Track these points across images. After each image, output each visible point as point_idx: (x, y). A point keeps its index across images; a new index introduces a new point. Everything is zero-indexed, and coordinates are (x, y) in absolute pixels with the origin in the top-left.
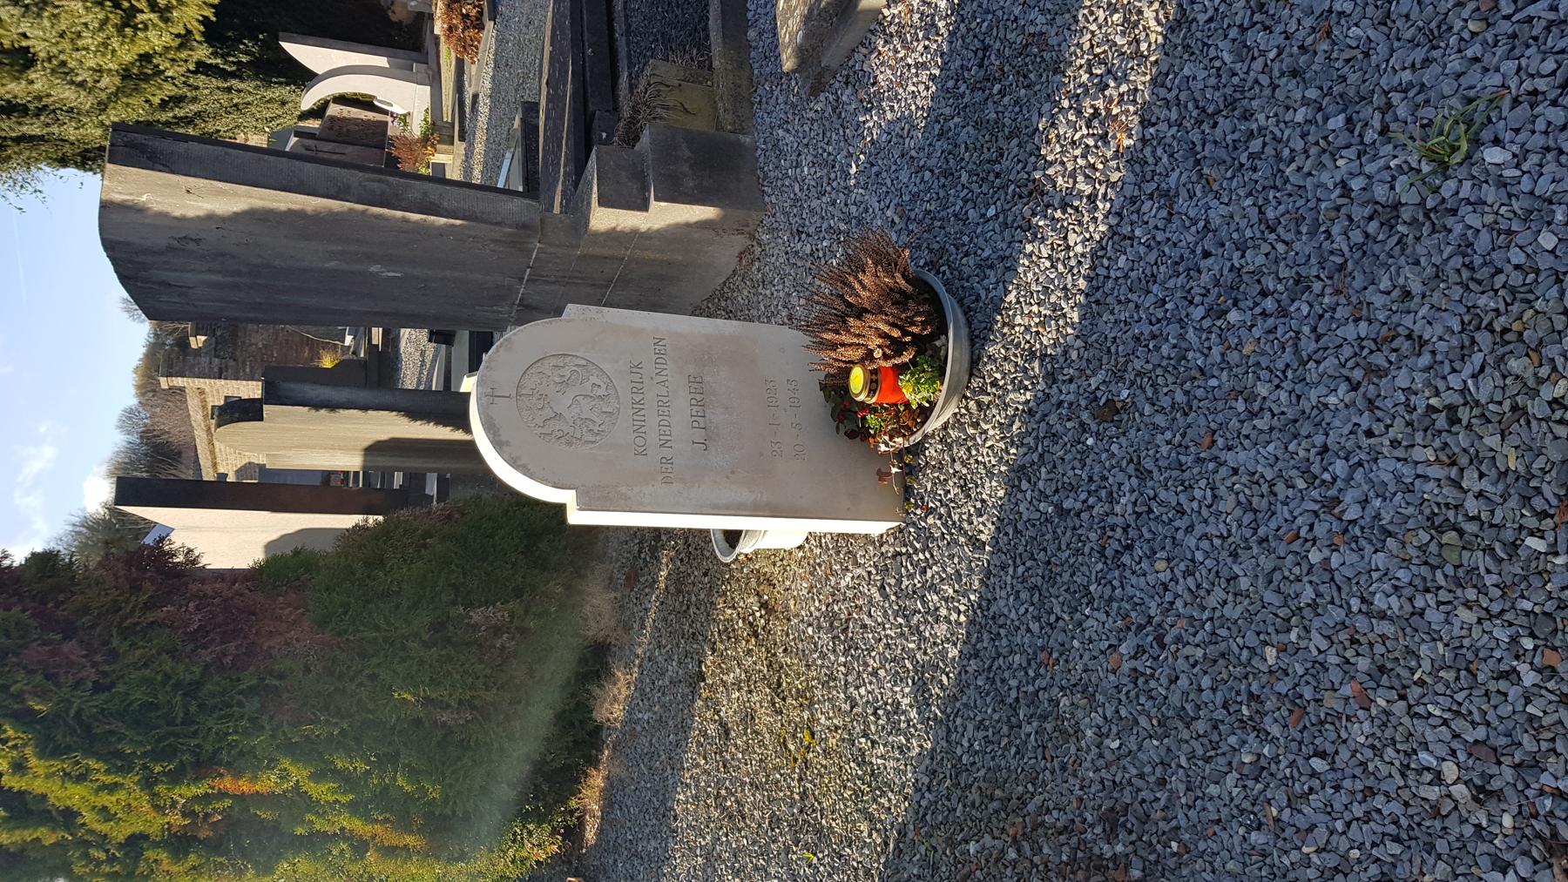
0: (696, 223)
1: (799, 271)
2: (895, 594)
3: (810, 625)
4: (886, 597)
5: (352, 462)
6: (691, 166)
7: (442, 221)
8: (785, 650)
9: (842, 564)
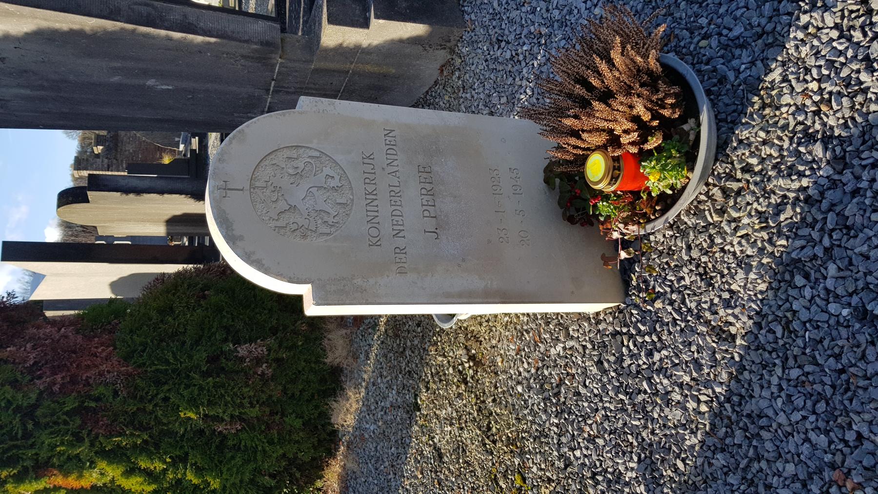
0: (408, 39)
1: (499, 75)
2: (615, 371)
3: (519, 383)
4: (605, 372)
5: (160, 230)
7: (199, 39)
8: (494, 401)
9: (551, 334)
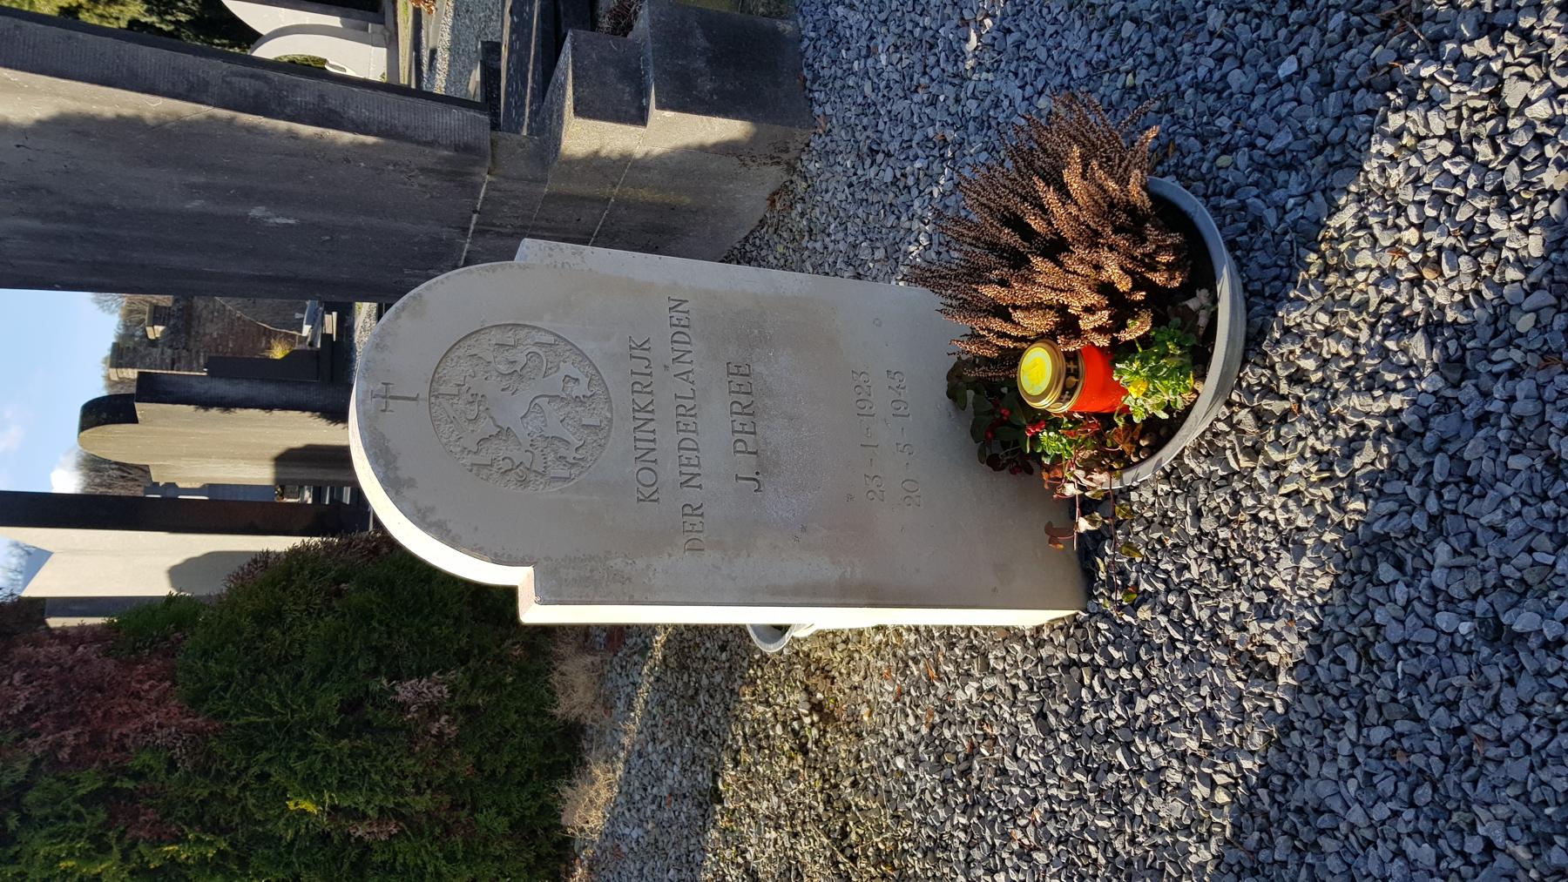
0: (715, 145)
2: (1067, 730)
3: (899, 752)
4: (1050, 732)
5: (261, 474)
6: (708, 62)
7: (347, 137)
8: (854, 784)
